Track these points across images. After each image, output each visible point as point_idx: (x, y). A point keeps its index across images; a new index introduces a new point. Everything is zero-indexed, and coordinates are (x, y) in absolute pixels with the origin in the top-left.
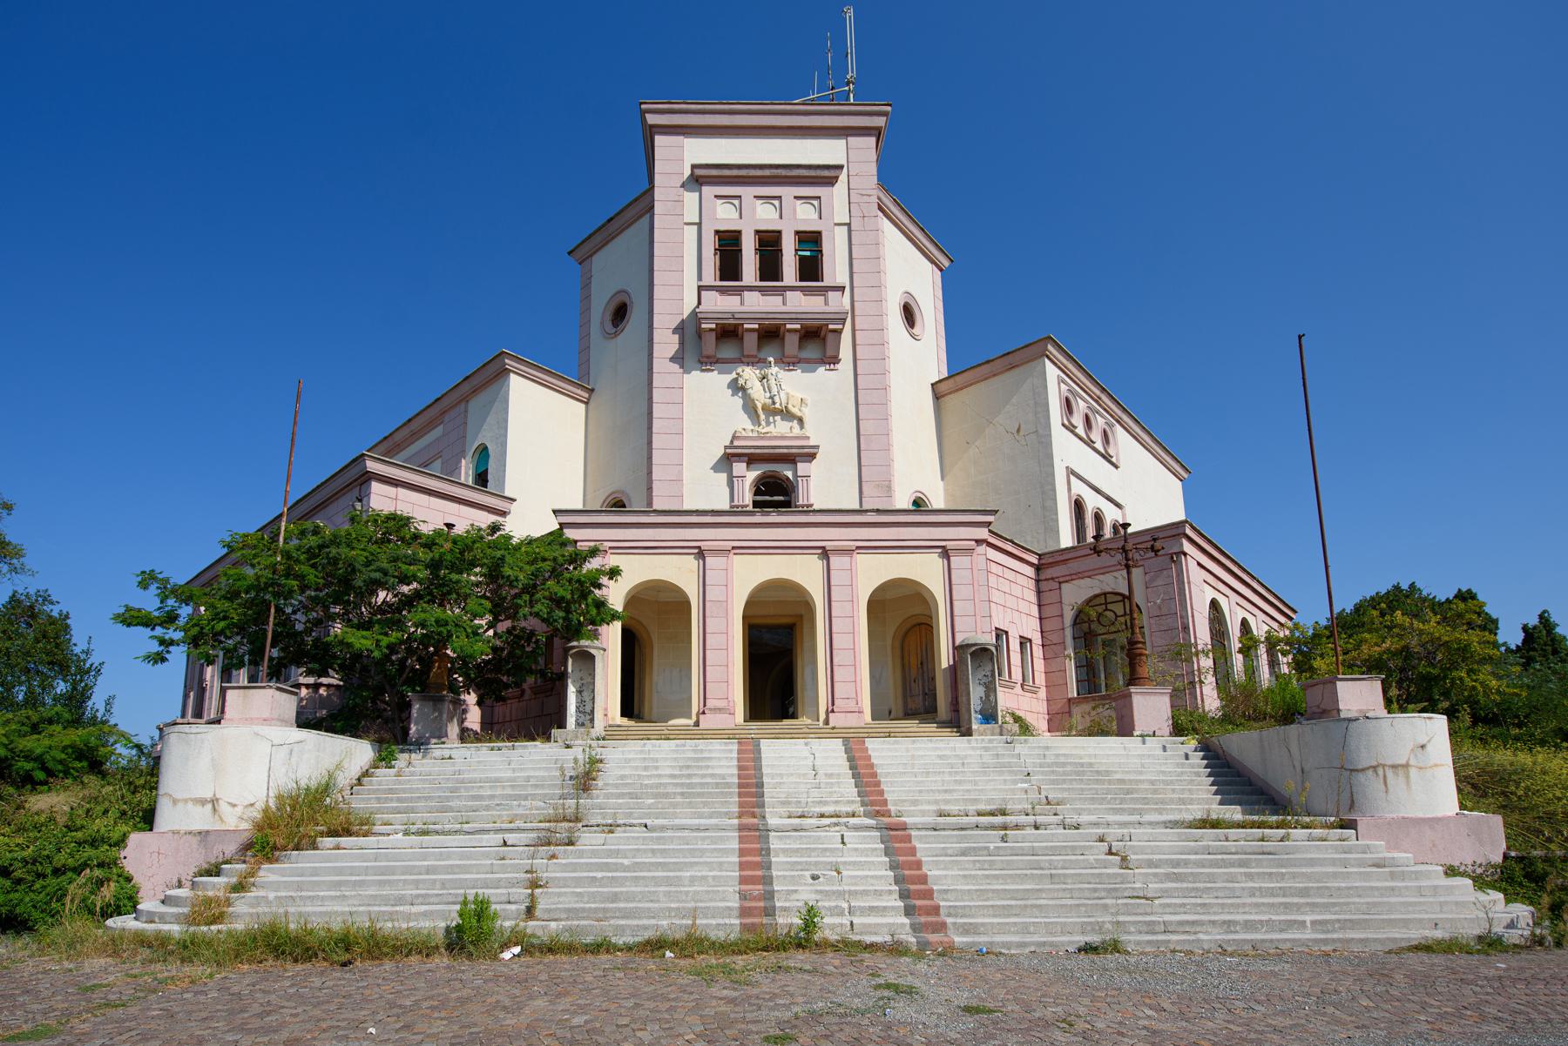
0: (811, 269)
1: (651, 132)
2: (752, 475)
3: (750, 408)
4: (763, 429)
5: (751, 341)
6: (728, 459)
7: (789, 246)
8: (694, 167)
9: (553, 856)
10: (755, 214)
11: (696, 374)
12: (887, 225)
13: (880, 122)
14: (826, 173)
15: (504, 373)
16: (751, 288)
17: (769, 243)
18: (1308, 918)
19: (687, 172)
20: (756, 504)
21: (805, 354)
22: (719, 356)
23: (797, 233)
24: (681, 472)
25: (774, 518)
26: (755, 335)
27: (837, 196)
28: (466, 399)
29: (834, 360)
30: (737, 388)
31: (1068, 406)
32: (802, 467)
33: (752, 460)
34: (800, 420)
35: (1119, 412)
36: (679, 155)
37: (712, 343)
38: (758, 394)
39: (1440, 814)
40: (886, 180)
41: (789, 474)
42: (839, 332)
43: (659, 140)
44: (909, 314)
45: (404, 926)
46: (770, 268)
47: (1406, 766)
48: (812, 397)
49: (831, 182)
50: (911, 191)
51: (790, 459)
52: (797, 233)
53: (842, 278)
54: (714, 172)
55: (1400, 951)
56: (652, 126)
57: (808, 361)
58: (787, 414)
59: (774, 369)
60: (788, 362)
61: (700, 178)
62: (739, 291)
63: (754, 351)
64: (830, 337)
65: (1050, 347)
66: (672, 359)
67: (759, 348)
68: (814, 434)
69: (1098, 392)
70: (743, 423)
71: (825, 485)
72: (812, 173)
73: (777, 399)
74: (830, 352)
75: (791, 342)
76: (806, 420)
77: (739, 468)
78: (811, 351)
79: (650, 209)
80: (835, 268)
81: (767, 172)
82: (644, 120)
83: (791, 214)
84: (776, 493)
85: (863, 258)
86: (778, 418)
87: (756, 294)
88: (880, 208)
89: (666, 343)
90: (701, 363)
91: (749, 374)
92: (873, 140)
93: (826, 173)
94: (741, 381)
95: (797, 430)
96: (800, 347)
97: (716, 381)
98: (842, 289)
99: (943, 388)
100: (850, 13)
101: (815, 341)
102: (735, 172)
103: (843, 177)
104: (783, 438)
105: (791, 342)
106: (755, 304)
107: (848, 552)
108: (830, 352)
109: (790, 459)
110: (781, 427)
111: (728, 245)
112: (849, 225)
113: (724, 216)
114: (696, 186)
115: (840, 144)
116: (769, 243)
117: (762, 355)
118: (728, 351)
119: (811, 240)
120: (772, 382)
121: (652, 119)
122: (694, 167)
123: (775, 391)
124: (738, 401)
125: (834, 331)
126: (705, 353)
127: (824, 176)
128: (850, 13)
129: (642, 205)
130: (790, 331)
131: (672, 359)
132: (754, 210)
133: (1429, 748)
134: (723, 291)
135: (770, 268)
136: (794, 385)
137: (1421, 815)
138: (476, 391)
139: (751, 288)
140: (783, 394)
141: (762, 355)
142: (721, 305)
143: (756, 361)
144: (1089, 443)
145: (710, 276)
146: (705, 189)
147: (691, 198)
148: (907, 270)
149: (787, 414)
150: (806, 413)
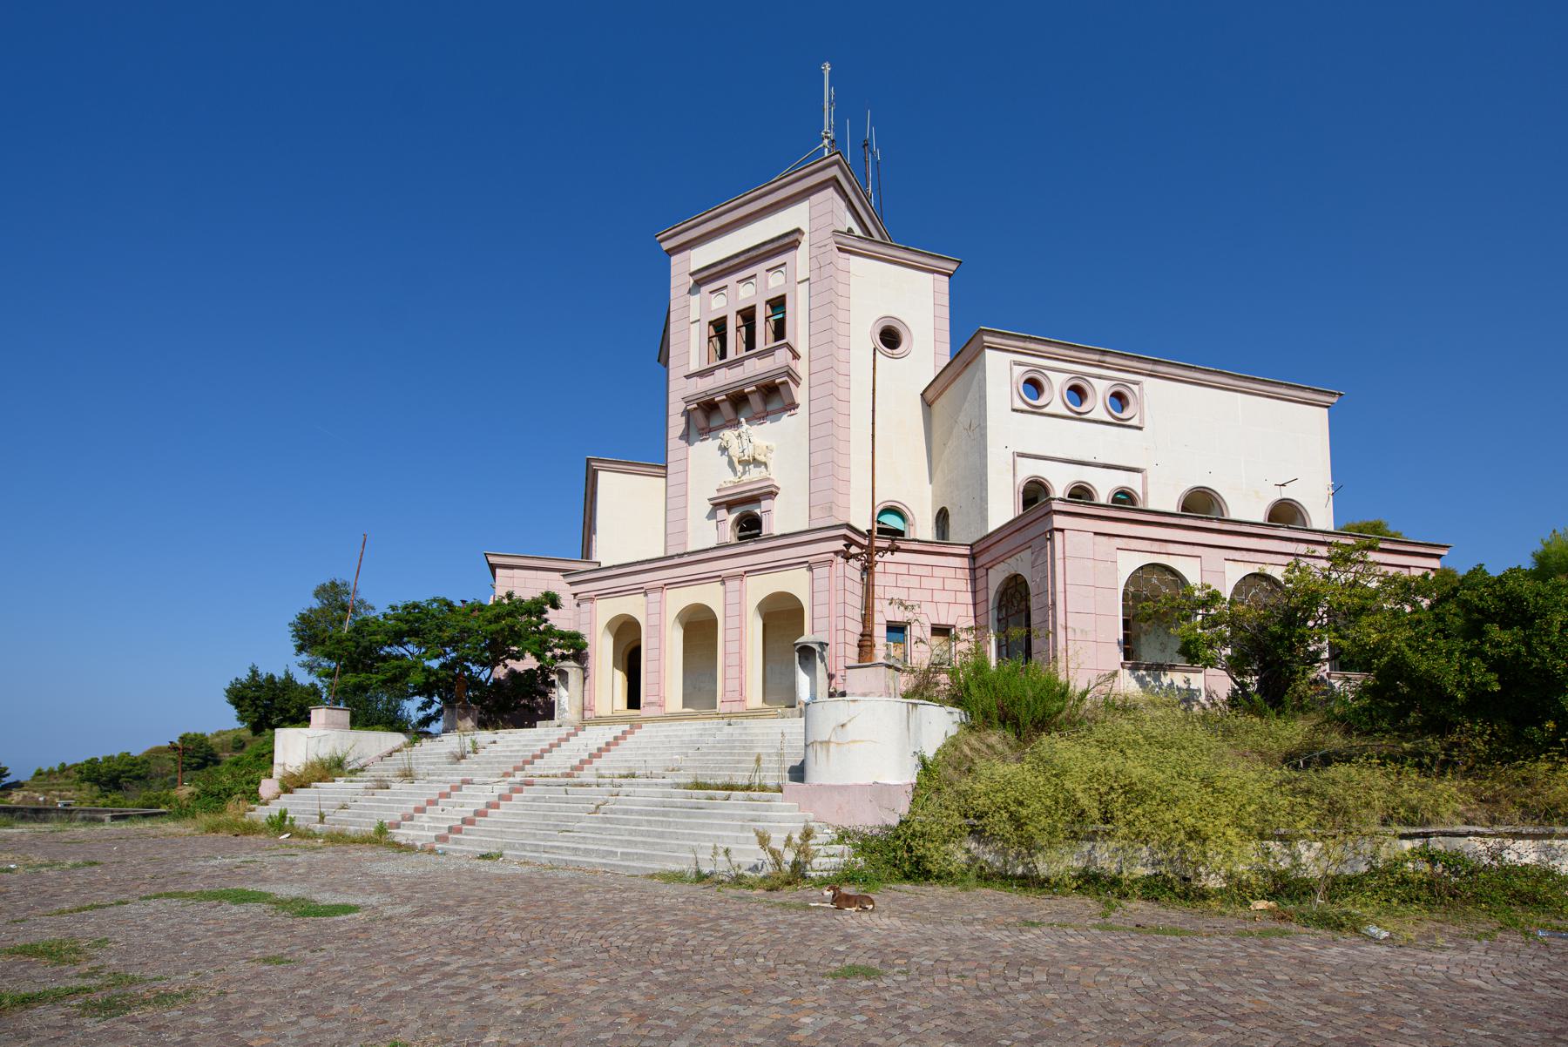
2: (732, 517)
4: (745, 478)
5: (726, 409)
9: (1021, 804)
11: (698, 444)
14: (787, 240)
18: (619, 850)
20: (740, 538)
21: (770, 408)
24: (685, 525)
25: (751, 546)
27: (800, 259)
30: (724, 449)
32: (765, 504)
33: (730, 506)
35: (1149, 367)
39: (850, 783)
47: (828, 742)
49: (794, 245)
51: (755, 500)
52: (783, 297)
54: (705, 274)
55: (652, 876)
57: (774, 412)
58: (756, 462)
59: (745, 426)
61: (704, 278)
63: (732, 416)
65: (986, 338)
66: (681, 438)
69: (1097, 357)
70: (730, 477)
71: (778, 518)
72: (776, 245)
75: (756, 402)
77: (722, 513)
84: (750, 526)
89: (677, 424)
91: (728, 435)
93: (787, 240)
100: (827, 68)
105: (756, 402)
107: (741, 576)
109: (755, 500)
110: (755, 473)
111: (719, 326)
115: (803, 207)
127: (789, 242)
131: (681, 438)
133: (849, 726)
136: (756, 437)
137: (833, 782)
142: (725, 378)
149: (756, 462)
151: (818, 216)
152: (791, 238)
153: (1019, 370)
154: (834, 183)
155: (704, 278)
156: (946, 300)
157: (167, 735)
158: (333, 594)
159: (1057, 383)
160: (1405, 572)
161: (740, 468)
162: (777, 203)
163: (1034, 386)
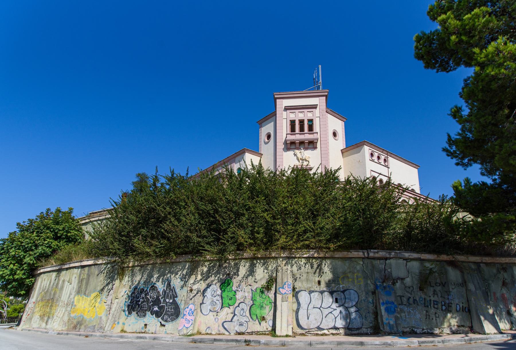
0: (311, 128)
1: (276, 99)
3: (298, 159)
5: (297, 145)
7: (306, 123)
10: (298, 116)
12: (329, 115)
13: (326, 94)
15: (244, 152)
17: (302, 122)
21: (310, 147)
27: (317, 111)
28: (235, 157)
29: (316, 148)
30: (295, 155)
31: (372, 155)
36: (282, 103)
37: (290, 145)
38: (299, 156)
42: (317, 142)
43: (277, 100)
44: (335, 134)
45: (289, 161)
46: (302, 129)
49: (316, 108)
50: (333, 108)
59: (303, 151)
60: (306, 149)
61: (287, 109)
62: (295, 134)
75: (306, 145)
78: (311, 146)
79: (276, 115)
80: (317, 127)
85: (324, 125)
91: (297, 152)
97: (291, 153)
99: (343, 151)
100: (320, 66)
101: (312, 144)
103: (318, 106)
105: (306, 145)
106: (298, 137)
110: (305, 163)
111: (293, 123)
113: (292, 116)
115: (317, 99)
116: (302, 122)
118: (293, 147)
119: (311, 121)
121: (276, 96)
124: (295, 157)
127: (314, 107)
128: (320, 66)
129: (274, 114)
134: (291, 134)
135: (302, 129)
136: (307, 154)
138: (237, 156)
143: (299, 149)
144: (380, 163)
145: (289, 132)
147: (285, 113)
148: (337, 124)
150: (310, 160)
153: (370, 151)
154: (326, 96)
156: (344, 130)
158: (142, 178)
159: (376, 155)
160: (380, 324)
161: (301, 161)
163: (372, 155)
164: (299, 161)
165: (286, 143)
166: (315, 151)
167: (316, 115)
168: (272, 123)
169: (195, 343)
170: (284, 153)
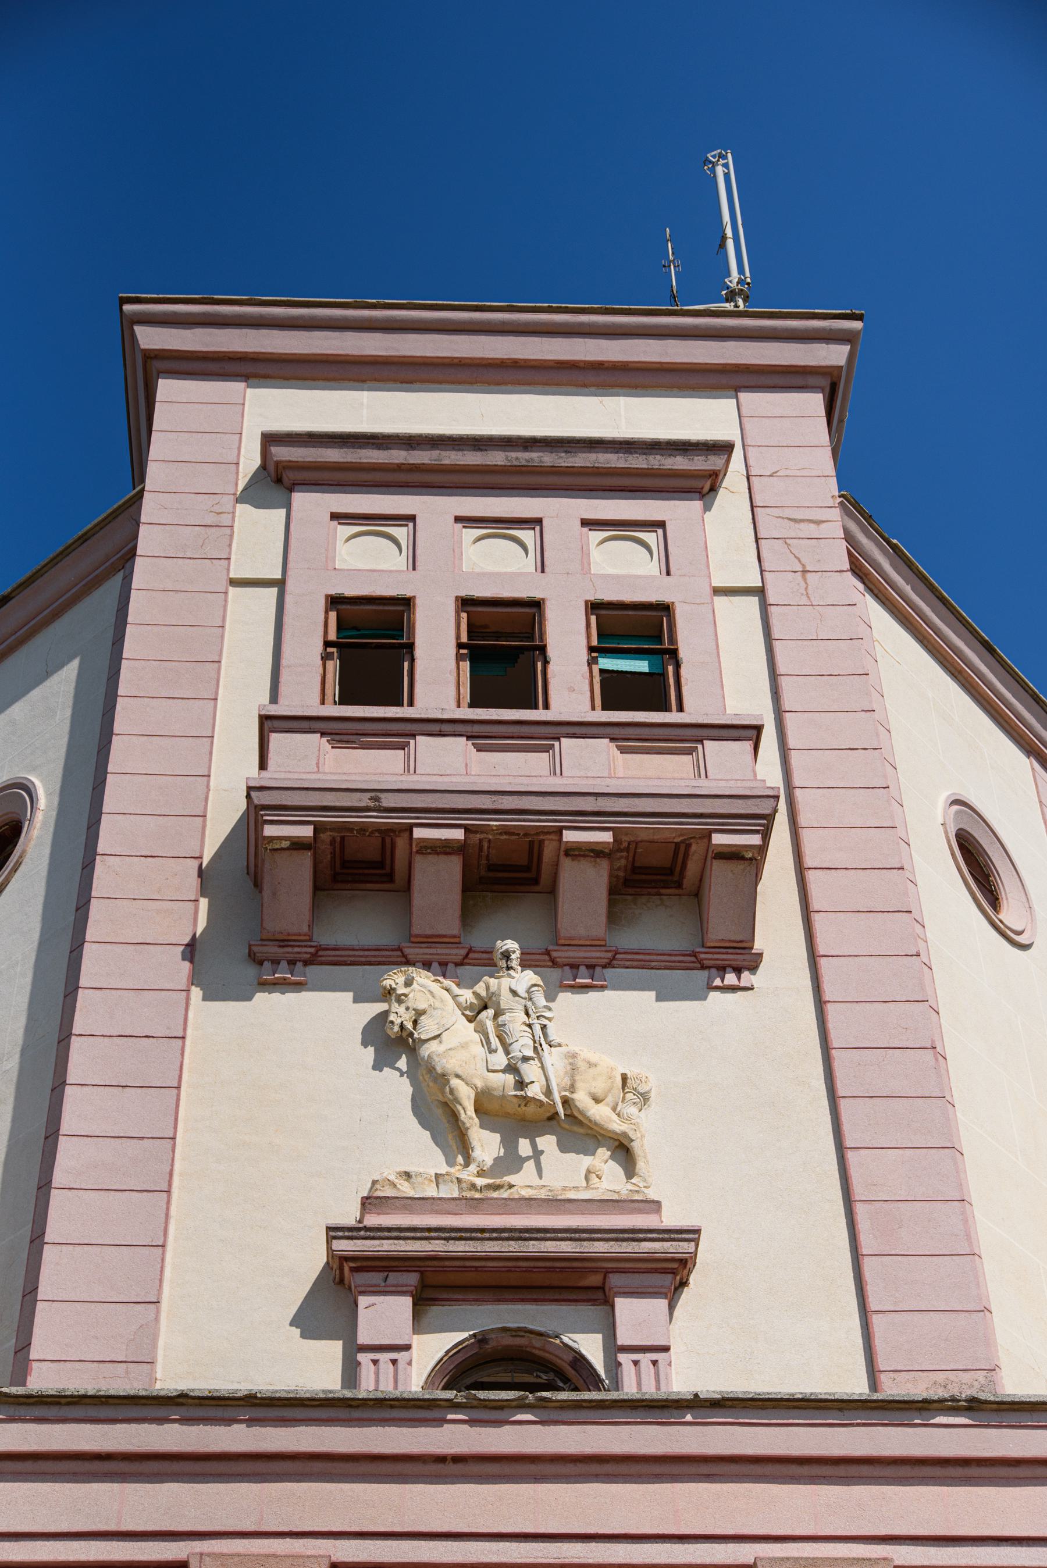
3: (437, 1110)
5: (437, 888)
6: (348, 1275)
8: (269, 440)
10: (447, 561)
13: (836, 355)
16: (439, 727)
19: (251, 460)
21: (628, 939)
22: (326, 937)
23: (594, 607)
24: (150, 1332)
26: (453, 867)
27: (718, 535)
30: (393, 1043)
32: (635, 1316)
33: (435, 1283)
34: (623, 1151)
40: (863, 493)
41: (590, 1347)
42: (752, 861)
43: (167, 388)
48: (680, 1092)
49: (703, 487)
53: (744, 698)
56: (152, 356)
58: (575, 1129)
59: (525, 979)
60: (573, 966)
62: (399, 735)
63: (449, 923)
64: (720, 874)
67: (468, 915)
68: (675, 1188)
70: (410, 1157)
73: (531, 1071)
74: (719, 930)
75: (583, 893)
76: (643, 1147)
78: (656, 929)
79: (126, 557)
81: (497, 458)
82: (129, 340)
83: (573, 564)
86: (547, 1142)
87: (460, 745)
88: (857, 570)
89: (150, 898)
90: (256, 959)
91: (430, 998)
92: (816, 401)
94: (400, 1015)
95: (610, 1180)
96: (613, 918)
97: (324, 1018)
98: (752, 732)
101: (669, 896)
102: (398, 456)
104: (556, 1204)
106: (446, 768)
108: (719, 930)
110: (559, 1172)
111: (369, 643)
112: (760, 592)
113: (368, 564)
114: (278, 493)
117: (477, 940)
118: (358, 924)
120: (515, 1020)
121: (149, 338)
122: (269, 440)
123: (523, 1045)
124: (396, 1086)
125: (732, 855)
126: (274, 926)
129: (101, 549)
130: (576, 852)
132: (456, 552)
136: (602, 1036)
139: (439, 727)
140: (553, 1058)
141: (477, 940)
143: (459, 958)
145: (308, 689)
146: (299, 498)
149: (575, 1129)
150: (647, 1129)
151: (783, 447)
152: (699, 463)
154: (832, 385)
155: (285, 472)
157: (691, 1280)
161: (486, 1145)
162: (598, 367)
164: (455, 1140)
165: (244, 868)
166: (718, 1012)
167: (707, 561)
168: (64, 681)
169: (967, 1221)
170: (211, 1020)
